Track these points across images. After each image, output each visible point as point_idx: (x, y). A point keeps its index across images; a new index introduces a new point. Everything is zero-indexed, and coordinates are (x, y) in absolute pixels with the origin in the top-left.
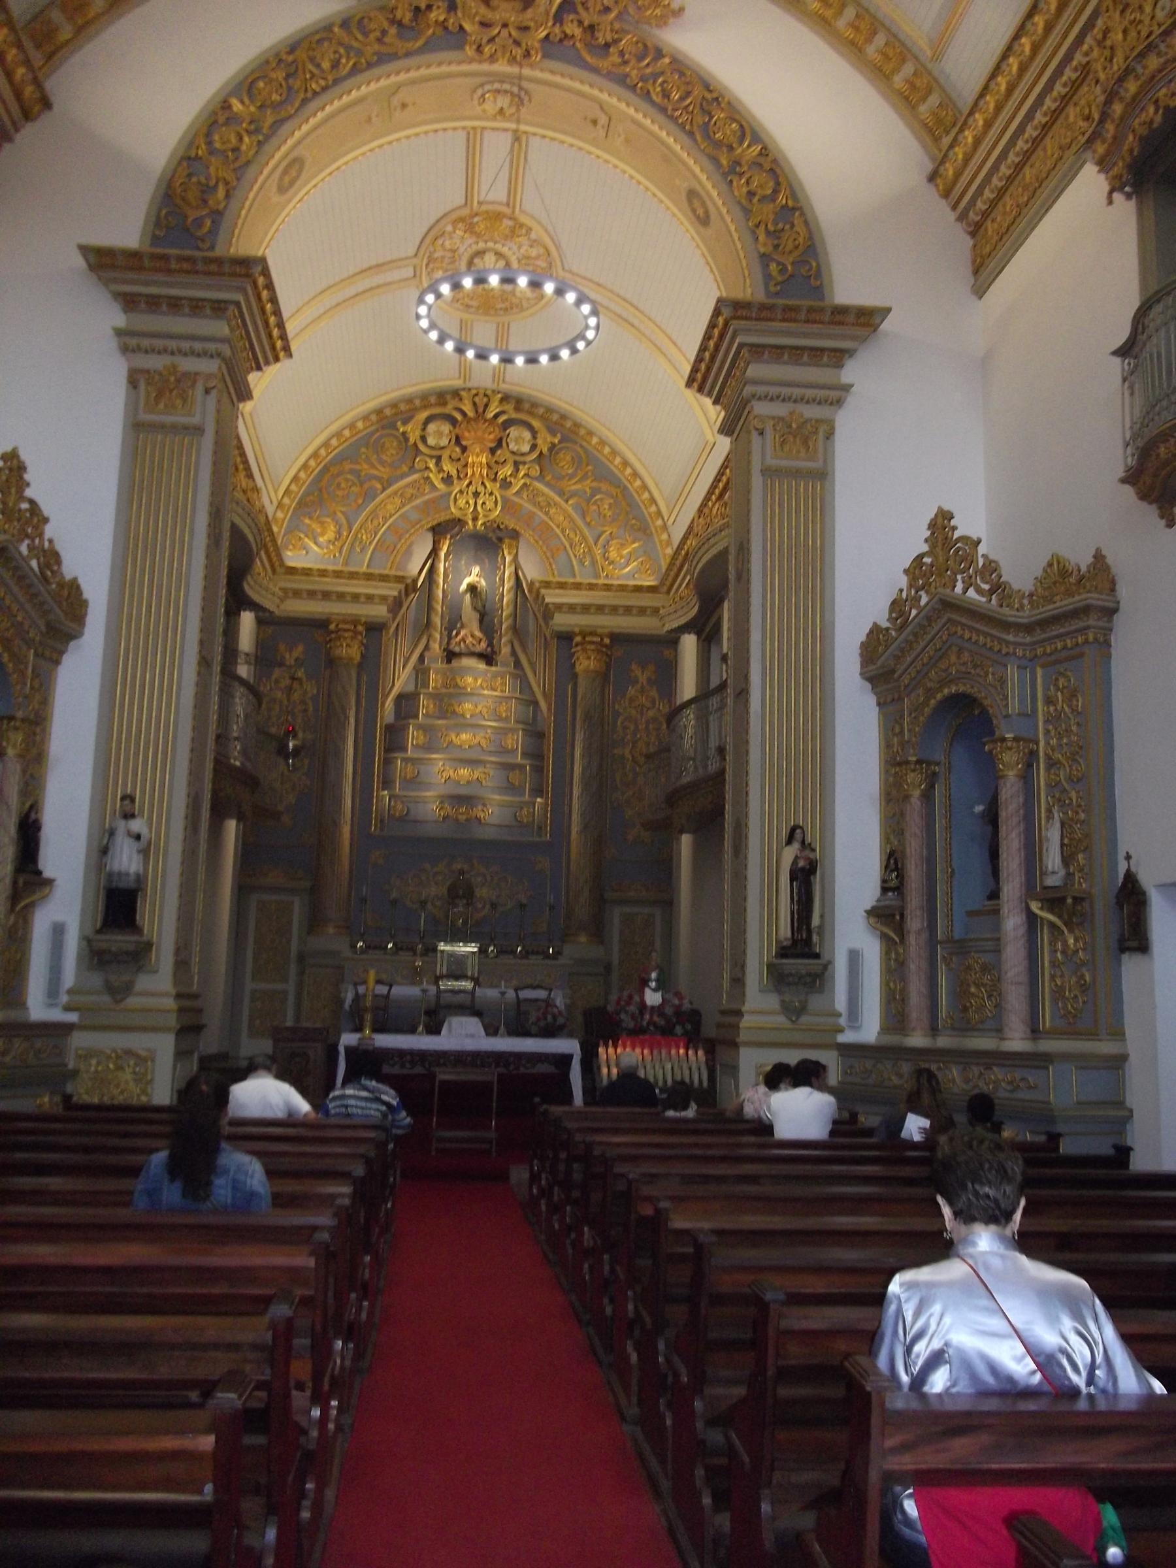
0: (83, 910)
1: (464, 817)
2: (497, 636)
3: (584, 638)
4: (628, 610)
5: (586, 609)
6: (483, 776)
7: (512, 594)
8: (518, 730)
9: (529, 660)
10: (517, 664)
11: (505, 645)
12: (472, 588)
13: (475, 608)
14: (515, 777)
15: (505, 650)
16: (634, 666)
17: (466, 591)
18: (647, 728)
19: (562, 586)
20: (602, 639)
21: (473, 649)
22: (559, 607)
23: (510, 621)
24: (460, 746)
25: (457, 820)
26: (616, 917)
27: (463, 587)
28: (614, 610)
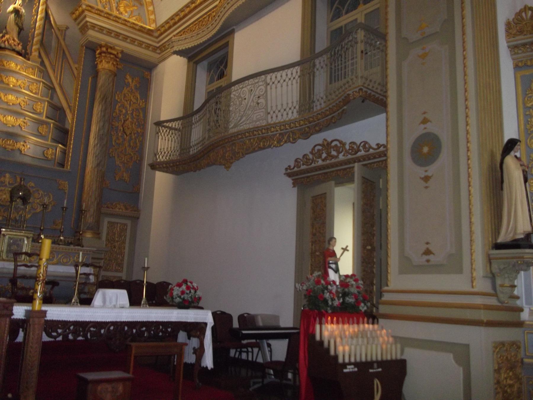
0: (492, 305)
1: (11, 147)
2: (30, 44)
3: (107, 49)
4: (133, 41)
5: (109, 32)
6: (22, 123)
7: (42, 22)
8: (44, 101)
9: (50, 63)
10: (42, 63)
11: (35, 51)
12: (16, 11)
13: (17, 24)
14: (43, 130)
15: (35, 54)
16: (128, 77)
17: (12, 12)
18: (132, 114)
19: (99, 13)
20: (117, 54)
21: (14, 47)
22: (94, 26)
23: (40, 37)
24: (7, 103)
25: (5, 148)
26: (105, 222)
27: (11, 8)
28: (125, 38)
